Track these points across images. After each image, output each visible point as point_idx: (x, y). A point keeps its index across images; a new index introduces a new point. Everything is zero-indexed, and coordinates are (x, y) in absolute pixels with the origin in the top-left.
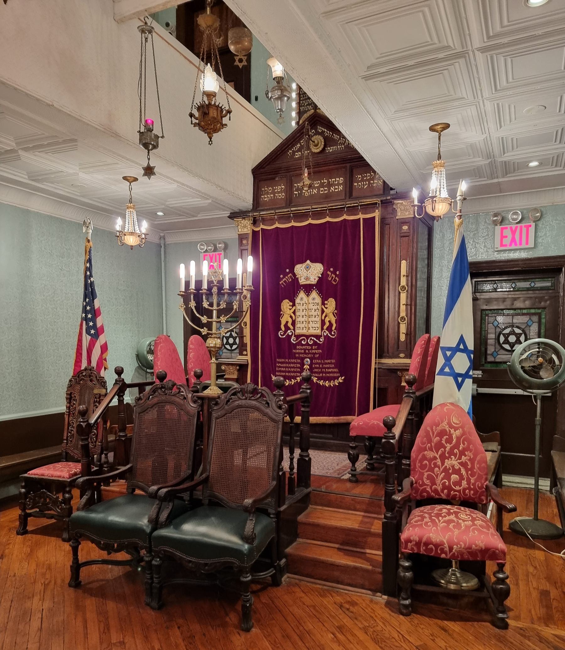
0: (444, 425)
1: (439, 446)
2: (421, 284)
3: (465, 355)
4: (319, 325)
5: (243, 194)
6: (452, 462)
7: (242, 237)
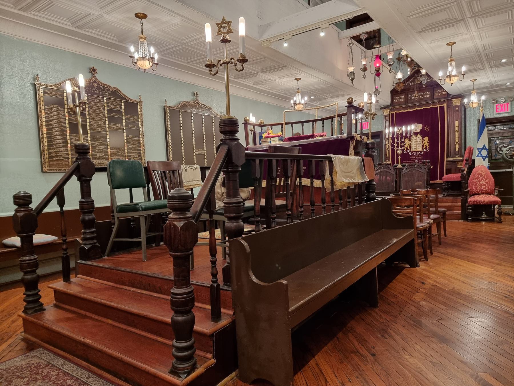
0: (480, 171)
1: (478, 178)
2: (463, 129)
3: (485, 150)
4: (421, 147)
5: (387, 100)
6: (483, 182)
7: (385, 116)
